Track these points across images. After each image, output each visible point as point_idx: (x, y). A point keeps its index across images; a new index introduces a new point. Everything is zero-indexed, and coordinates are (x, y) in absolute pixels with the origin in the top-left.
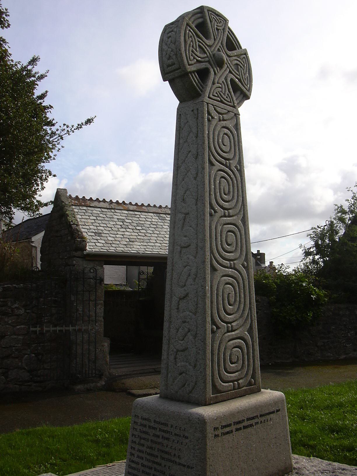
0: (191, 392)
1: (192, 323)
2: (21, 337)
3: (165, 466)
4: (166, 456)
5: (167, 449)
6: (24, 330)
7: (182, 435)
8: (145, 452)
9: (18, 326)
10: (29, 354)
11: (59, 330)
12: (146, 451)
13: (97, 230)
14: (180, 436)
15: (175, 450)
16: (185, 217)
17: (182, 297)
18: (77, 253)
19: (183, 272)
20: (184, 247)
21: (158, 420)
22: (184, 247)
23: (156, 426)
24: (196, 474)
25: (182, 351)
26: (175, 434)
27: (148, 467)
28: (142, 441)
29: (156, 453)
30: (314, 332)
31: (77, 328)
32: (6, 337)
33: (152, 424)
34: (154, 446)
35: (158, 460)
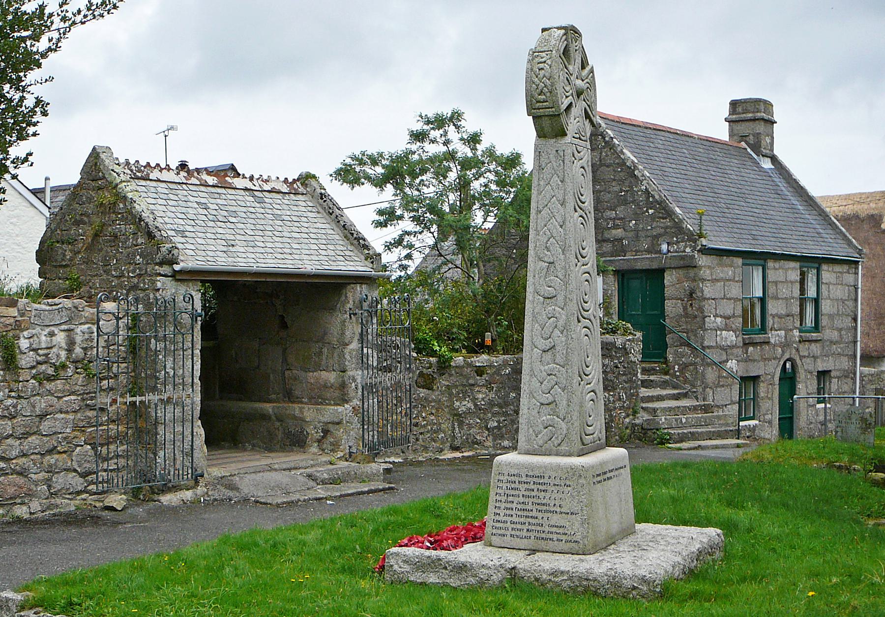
0: (559, 445)
1: (560, 376)
2: (71, 416)
3: (543, 518)
4: (544, 508)
5: (544, 501)
6: (74, 403)
7: (563, 484)
8: (514, 508)
9: (65, 396)
10: (82, 446)
11: (130, 402)
12: (516, 508)
13: (177, 225)
14: (561, 485)
15: (555, 500)
16: (548, 266)
17: (546, 350)
18: (163, 269)
19: (548, 324)
20: (548, 298)
21: (531, 473)
22: (548, 298)
23: (529, 480)
24: (582, 519)
25: (547, 404)
26: (555, 485)
27: (519, 523)
28: (510, 498)
29: (529, 507)
30: (483, 403)
31: (165, 397)
32: (48, 417)
33: (524, 479)
34: (527, 500)
35: (534, 514)
